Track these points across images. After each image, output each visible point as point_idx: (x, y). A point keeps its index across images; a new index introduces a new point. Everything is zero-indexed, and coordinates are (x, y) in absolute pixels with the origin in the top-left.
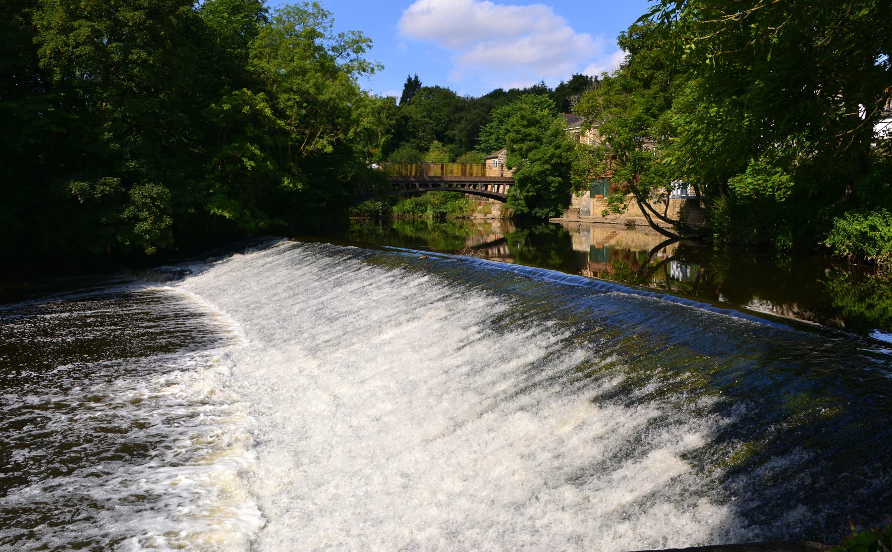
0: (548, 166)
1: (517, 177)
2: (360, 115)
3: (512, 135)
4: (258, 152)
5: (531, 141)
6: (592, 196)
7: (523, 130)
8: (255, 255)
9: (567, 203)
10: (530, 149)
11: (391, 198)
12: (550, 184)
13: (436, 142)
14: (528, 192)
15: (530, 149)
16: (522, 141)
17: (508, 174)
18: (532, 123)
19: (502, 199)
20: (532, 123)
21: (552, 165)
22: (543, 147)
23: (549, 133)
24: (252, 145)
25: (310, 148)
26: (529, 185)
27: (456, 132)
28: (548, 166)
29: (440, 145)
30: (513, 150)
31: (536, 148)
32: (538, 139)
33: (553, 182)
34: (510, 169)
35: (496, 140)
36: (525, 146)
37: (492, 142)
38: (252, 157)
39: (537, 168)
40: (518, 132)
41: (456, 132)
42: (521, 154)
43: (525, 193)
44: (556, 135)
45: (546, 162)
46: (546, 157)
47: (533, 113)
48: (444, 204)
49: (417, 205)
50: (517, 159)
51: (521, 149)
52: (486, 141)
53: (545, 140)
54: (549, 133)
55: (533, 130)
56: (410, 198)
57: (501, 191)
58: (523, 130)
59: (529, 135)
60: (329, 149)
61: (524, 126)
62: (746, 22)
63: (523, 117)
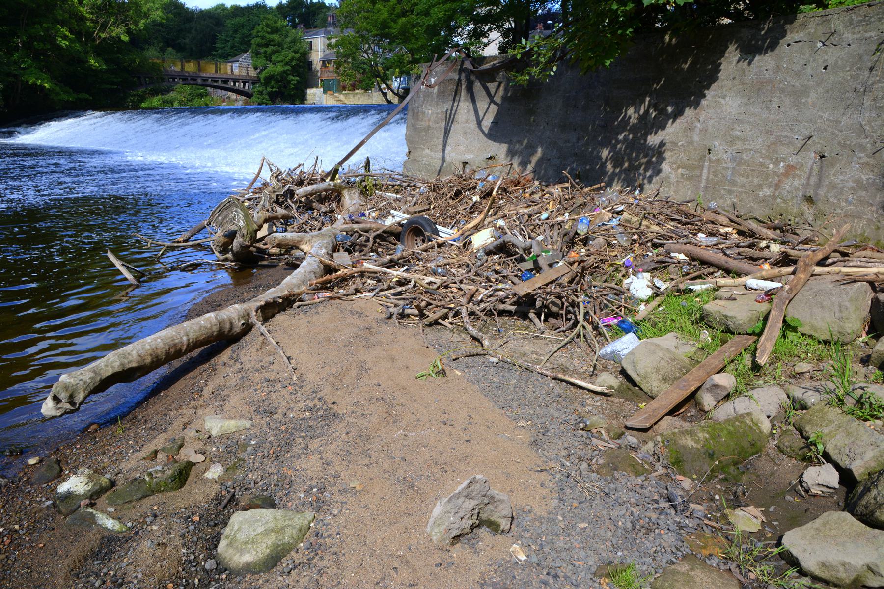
0: (289, 67)
1: (262, 76)
2: (149, 10)
3: (258, 40)
4: (67, 33)
5: (274, 46)
6: (325, 92)
7: (267, 36)
8: (70, 121)
9: (303, 98)
10: (274, 52)
11: (139, 96)
12: (289, 82)
13: (170, 49)
14: (272, 88)
15: (274, 52)
16: (266, 45)
17: (253, 73)
18: (276, 31)
19: (248, 95)
20: (276, 31)
21: (292, 67)
22: (284, 52)
23: (288, 40)
24: (63, 27)
25: (103, 35)
26: (273, 83)
27: (187, 41)
28: (289, 67)
29: (174, 52)
30: (257, 54)
31: (278, 51)
32: (280, 45)
33: (293, 80)
34: (256, 69)
35: (232, 48)
36: (270, 49)
37: (228, 49)
38: (65, 37)
39: (280, 68)
40: (263, 38)
41: (187, 41)
42: (265, 57)
43: (269, 89)
44: (294, 42)
45: (287, 64)
46: (287, 60)
47: (276, 22)
48: (190, 101)
49: (164, 102)
50: (261, 62)
51: (265, 52)
52: (222, 48)
53: (286, 46)
54: (288, 40)
55: (276, 37)
56: (157, 95)
57: (246, 87)
58: (267, 36)
59: (273, 41)
60: (125, 38)
61: (268, 33)
62: (557, 217)
63: (267, 26)
